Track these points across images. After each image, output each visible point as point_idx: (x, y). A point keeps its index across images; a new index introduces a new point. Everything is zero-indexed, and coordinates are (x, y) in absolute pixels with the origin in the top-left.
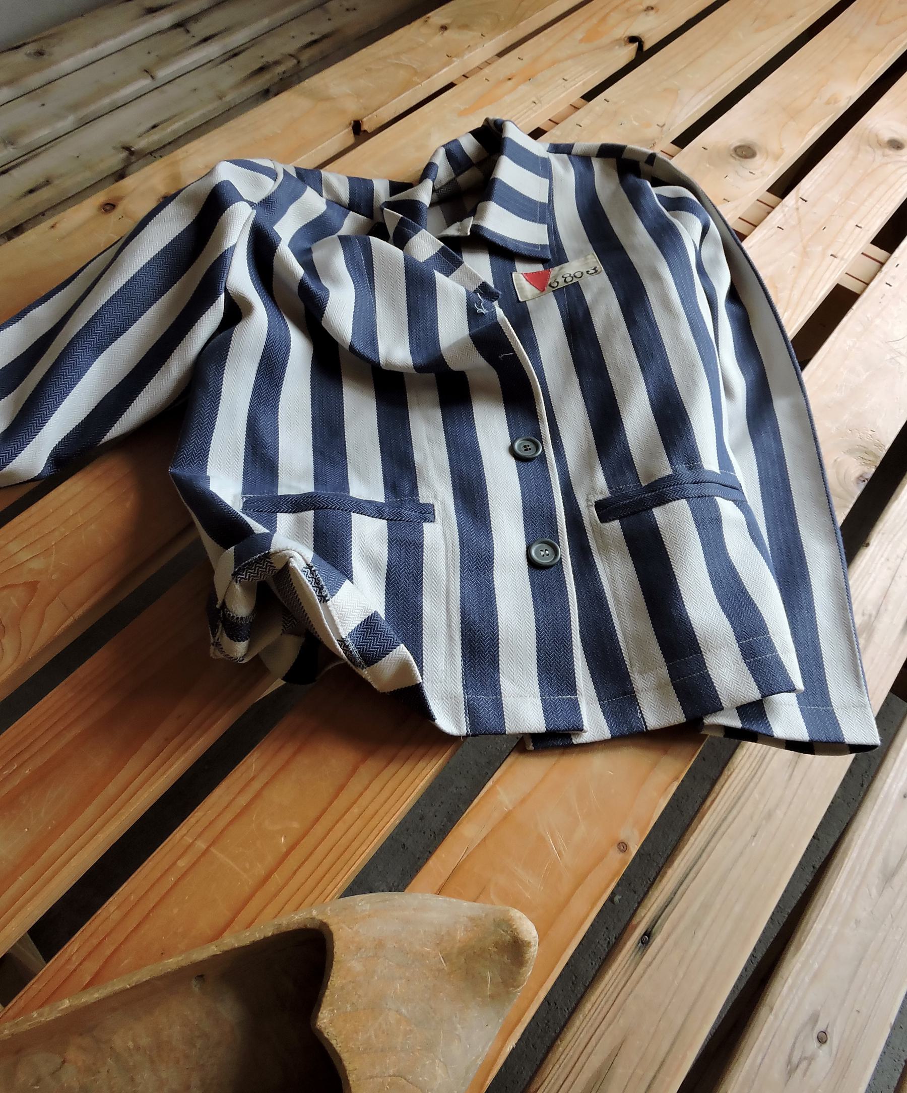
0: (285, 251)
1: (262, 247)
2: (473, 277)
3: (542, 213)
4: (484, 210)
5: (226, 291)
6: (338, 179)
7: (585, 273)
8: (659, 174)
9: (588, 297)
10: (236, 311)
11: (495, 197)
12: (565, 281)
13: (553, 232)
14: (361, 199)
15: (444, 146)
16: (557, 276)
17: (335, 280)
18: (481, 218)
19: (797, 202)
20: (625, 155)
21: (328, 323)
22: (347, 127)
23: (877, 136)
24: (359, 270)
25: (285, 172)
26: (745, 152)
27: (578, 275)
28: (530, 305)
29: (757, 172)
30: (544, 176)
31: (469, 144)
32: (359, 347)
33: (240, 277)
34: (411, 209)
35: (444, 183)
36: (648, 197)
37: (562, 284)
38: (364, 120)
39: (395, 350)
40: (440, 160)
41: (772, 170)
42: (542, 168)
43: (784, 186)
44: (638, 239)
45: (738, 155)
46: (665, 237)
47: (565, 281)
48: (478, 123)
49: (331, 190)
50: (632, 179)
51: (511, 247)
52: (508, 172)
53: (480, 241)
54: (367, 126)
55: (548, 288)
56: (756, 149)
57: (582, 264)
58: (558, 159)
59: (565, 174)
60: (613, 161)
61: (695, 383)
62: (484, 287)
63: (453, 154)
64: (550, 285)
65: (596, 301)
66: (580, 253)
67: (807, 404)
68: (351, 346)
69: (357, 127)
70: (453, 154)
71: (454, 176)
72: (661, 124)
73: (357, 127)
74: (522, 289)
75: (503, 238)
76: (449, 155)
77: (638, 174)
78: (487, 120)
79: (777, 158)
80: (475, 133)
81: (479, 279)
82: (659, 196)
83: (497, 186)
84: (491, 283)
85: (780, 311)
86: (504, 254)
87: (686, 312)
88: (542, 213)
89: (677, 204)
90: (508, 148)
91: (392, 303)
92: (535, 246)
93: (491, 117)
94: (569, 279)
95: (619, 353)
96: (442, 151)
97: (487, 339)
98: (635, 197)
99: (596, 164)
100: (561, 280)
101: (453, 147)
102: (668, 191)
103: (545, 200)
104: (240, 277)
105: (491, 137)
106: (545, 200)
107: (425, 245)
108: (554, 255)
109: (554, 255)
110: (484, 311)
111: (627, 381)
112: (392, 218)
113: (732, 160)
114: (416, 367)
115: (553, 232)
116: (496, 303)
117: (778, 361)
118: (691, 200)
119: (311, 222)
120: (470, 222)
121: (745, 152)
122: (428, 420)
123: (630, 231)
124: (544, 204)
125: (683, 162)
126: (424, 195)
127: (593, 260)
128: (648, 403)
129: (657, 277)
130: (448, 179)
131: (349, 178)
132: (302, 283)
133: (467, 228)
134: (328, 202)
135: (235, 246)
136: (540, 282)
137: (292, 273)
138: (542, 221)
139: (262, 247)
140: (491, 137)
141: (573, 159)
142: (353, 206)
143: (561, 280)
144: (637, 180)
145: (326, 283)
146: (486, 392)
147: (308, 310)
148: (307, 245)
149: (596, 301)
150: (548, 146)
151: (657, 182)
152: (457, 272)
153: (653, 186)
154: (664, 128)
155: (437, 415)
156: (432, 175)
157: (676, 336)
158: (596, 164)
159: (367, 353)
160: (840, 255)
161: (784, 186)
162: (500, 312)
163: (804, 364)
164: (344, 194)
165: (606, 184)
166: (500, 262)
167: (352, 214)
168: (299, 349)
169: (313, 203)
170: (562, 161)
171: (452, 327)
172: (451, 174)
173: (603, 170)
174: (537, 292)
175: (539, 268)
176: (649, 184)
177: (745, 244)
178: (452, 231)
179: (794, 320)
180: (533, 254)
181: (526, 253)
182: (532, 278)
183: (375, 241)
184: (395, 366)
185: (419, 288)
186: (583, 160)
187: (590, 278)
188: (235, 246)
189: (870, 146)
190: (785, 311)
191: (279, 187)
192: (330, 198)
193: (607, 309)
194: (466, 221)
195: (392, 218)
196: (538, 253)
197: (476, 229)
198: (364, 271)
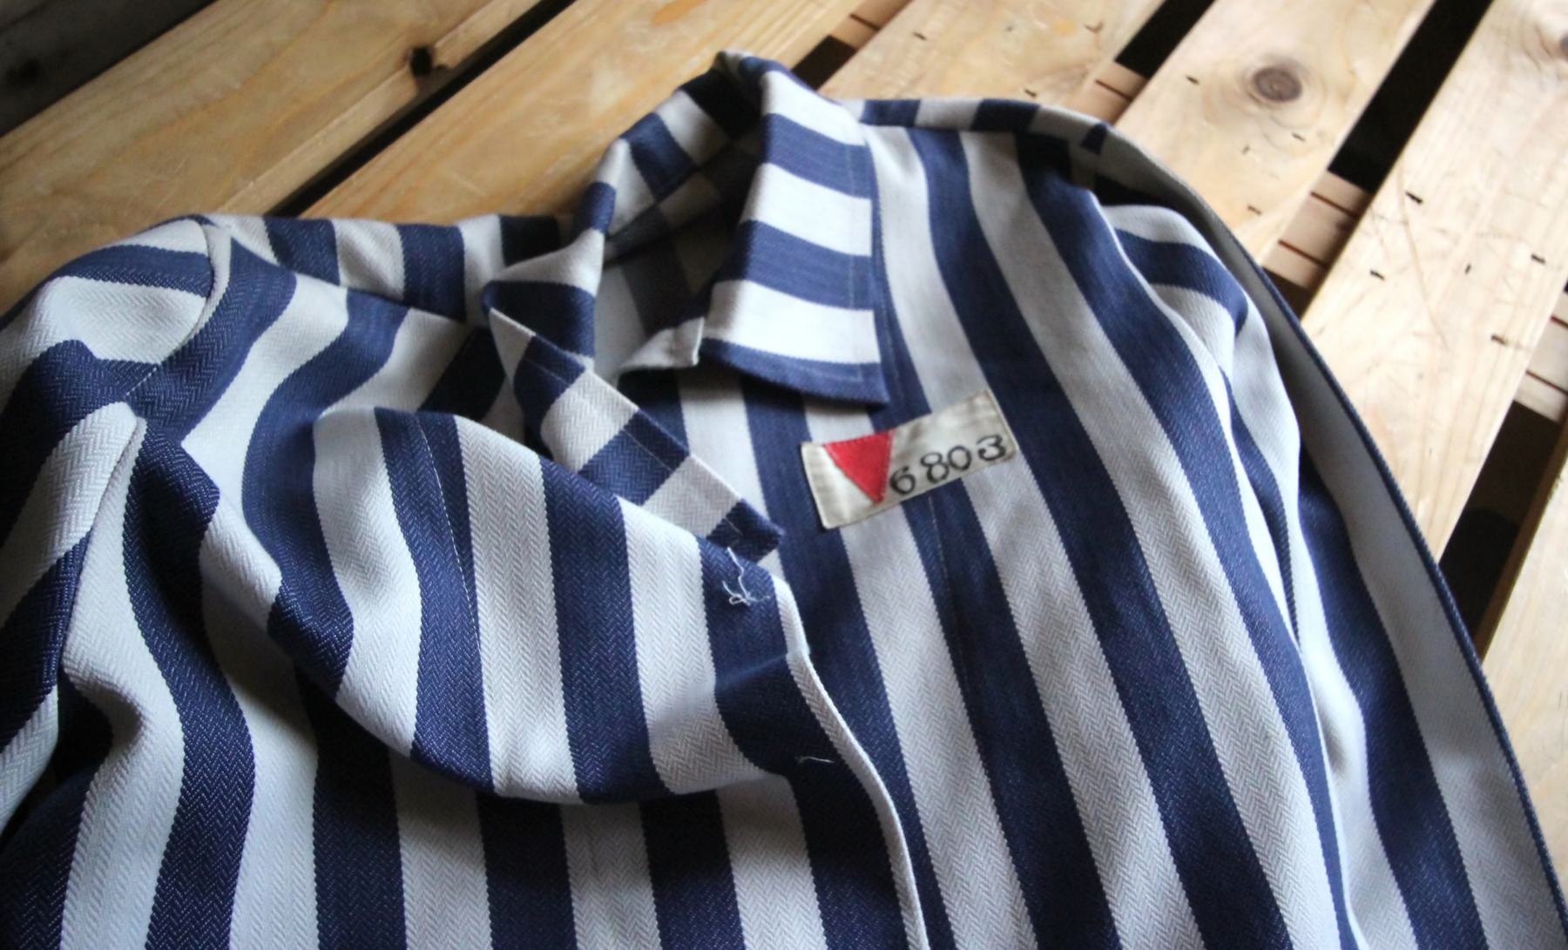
0: (231, 525)
1: (165, 511)
2: (714, 490)
3: (857, 282)
4: (728, 304)
5: (64, 680)
6: (377, 238)
7: (976, 458)
8: (1114, 171)
9: (992, 531)
10: (100, 726)
11: (753, 268)
12: (930, 477)
13: (887, 326)
14: (434, 270)
15: (625, 136)
16: (905, 455)
17: (370, 572)
18: (723, 320)
19: (1402, 203)
20: (1036, 127)
21: (354, 701)
22: (399, 67)
23: (1538, 29)
24: (432, 519)
25: (238, 251)
26: (1277, 85)
27: (959, 458)
28: (850, 538)
29: (1309, 135)
30: (859, 193)
31: (680, 118)
32: (437, 748)
33: (107, 632)
34: (556, 312)
35: (629, 217)
36: (1101, 245)
37: (923, 487)
38: (439, 45)
39: (531, 743)
40: (620, 175)
41: (1330, 120)
42: (849, 171)
43: (1368, 156)
44: (1095, 366)
45: (1264, 94)
46: (1159, 363)
47: (930, 477)
48: (699, 64)
49: (357, 264)
50: (1055, 185)
51: (794, 381)
52: (785, 202)
53: (720, 373)
54: (449, 54)
55: (889, 492)
56: (1300, 76)
57: (960, 425)
58: (886, 139)
59: (905, 179)
60: (1009, 139)
61: (1278, 796)
62: (741, 512)
63: (650, 148)
64: (894, 485)
65: (1010, 543)
66: (955, 387)
67: (1519, 782)
68: (417, 749)
69: (420, 61)
70: (650, 148)
71: (651, 200)
72: (1093, 24)
73: (420, 61)
74: (826, 490)
75: (775, 361)
76: (641, 157)
77: (1066, 168)
78: (721, 58)
79: (1345, 96)
80: (695, 89)
81: (728, 494)
82: (1124, 236)
83: (758, 241)
84: (758, 505)
85: (1408, 496)
86: (777, 398)
87: (1233, 584)
88: (857, 282)
89: (1171, 265)
90: (777, 142)
91: (518, 595)
92: (849, 369)
93: (732, 50)
94: (938, 471)
95: (1084, 702)
96: (622, 150)
97: (757, 707)
98: (1072, 238)
99: (972, 148)
100: (918, 472)
101: (646, 134)
102: (1144, 220)
103: (863, 248)
104: (107, 632)
105: (731, 93)
106: (863, 248)
107: (592, 414)
108: (891, 394)
109: (891, 394)
110: (747, 598)
111: (1112, 790)
112: (512, 334)
113: (1253, 108)
114: (583, 790)
115: (887, 326)
116: (771, 562)
117: (1418, 619)
118: (1202, 253)
119: (309, 364)
120: (697, 332)
121: (1277, 85)
122: (621, 921)
123: (1071, 340)
124: (858, 260)
125: (1152, 128)
126: (586, 267)
127: (989, 411)
128: (1166, 850)
129: (1156, 489)
130: (637, 209)
131: (405, 230)
132: (279, 611)
133: (690, 348)
134: (355, 301)
135: (86, 542)
136: (864, 463)
137: (245, 586)
138: (860, 303)
139: (165, 511)
140: (731, 93)
141: (918, 135)
142: (415, 295)
143: (918, 472)
144: (1069, 189)
145: (347, 585)
146: (763, 823)
147: (295, 665)
148: (300, 416)
149: (1010, 543)
150: (859, 108)
151: (1115, 195)
152: (674, 484)
153: (1105, 202)
154: (1104, 33)
155: (644, 905)
156: (603, 218)
157: (1217, 654)
158: (972, 148)
159: (460, 761)
160: (1511, 336)
161: (1368, 156)
162: (784, 593)
163: (1483, 645)
164: (389, 265)
165: (995, 198)
166: (774, 419)
167: (414, 316)
168: (277, 764)
169: (318, 311)
170: (895, 144)
171: (671, 655)
172: (641, 199)
173: (990, 164)
174: (863, 500)
175: (860, 427)
176: (1094, 200)
177: (1311, 323)
178: (655, 355)
179: (1438, 512)
180: (847, 394)
181: (828, 391)
182: (853, 458)
183: (468, 429)
184: (531, 791)
185: (587, 558)
186: (940, 140)
187: (988, 471)
188: (86, 542)
189: (1528, 54)
190: (1419, 496)
191: (217, 313)
192: (357, 284)
193: (1042, 573)
194: (688, 326)
195: (512, 334)
196: (856, 387)
197: (713, 349)
198: (442, 518)
